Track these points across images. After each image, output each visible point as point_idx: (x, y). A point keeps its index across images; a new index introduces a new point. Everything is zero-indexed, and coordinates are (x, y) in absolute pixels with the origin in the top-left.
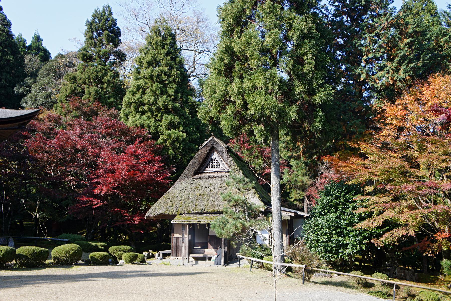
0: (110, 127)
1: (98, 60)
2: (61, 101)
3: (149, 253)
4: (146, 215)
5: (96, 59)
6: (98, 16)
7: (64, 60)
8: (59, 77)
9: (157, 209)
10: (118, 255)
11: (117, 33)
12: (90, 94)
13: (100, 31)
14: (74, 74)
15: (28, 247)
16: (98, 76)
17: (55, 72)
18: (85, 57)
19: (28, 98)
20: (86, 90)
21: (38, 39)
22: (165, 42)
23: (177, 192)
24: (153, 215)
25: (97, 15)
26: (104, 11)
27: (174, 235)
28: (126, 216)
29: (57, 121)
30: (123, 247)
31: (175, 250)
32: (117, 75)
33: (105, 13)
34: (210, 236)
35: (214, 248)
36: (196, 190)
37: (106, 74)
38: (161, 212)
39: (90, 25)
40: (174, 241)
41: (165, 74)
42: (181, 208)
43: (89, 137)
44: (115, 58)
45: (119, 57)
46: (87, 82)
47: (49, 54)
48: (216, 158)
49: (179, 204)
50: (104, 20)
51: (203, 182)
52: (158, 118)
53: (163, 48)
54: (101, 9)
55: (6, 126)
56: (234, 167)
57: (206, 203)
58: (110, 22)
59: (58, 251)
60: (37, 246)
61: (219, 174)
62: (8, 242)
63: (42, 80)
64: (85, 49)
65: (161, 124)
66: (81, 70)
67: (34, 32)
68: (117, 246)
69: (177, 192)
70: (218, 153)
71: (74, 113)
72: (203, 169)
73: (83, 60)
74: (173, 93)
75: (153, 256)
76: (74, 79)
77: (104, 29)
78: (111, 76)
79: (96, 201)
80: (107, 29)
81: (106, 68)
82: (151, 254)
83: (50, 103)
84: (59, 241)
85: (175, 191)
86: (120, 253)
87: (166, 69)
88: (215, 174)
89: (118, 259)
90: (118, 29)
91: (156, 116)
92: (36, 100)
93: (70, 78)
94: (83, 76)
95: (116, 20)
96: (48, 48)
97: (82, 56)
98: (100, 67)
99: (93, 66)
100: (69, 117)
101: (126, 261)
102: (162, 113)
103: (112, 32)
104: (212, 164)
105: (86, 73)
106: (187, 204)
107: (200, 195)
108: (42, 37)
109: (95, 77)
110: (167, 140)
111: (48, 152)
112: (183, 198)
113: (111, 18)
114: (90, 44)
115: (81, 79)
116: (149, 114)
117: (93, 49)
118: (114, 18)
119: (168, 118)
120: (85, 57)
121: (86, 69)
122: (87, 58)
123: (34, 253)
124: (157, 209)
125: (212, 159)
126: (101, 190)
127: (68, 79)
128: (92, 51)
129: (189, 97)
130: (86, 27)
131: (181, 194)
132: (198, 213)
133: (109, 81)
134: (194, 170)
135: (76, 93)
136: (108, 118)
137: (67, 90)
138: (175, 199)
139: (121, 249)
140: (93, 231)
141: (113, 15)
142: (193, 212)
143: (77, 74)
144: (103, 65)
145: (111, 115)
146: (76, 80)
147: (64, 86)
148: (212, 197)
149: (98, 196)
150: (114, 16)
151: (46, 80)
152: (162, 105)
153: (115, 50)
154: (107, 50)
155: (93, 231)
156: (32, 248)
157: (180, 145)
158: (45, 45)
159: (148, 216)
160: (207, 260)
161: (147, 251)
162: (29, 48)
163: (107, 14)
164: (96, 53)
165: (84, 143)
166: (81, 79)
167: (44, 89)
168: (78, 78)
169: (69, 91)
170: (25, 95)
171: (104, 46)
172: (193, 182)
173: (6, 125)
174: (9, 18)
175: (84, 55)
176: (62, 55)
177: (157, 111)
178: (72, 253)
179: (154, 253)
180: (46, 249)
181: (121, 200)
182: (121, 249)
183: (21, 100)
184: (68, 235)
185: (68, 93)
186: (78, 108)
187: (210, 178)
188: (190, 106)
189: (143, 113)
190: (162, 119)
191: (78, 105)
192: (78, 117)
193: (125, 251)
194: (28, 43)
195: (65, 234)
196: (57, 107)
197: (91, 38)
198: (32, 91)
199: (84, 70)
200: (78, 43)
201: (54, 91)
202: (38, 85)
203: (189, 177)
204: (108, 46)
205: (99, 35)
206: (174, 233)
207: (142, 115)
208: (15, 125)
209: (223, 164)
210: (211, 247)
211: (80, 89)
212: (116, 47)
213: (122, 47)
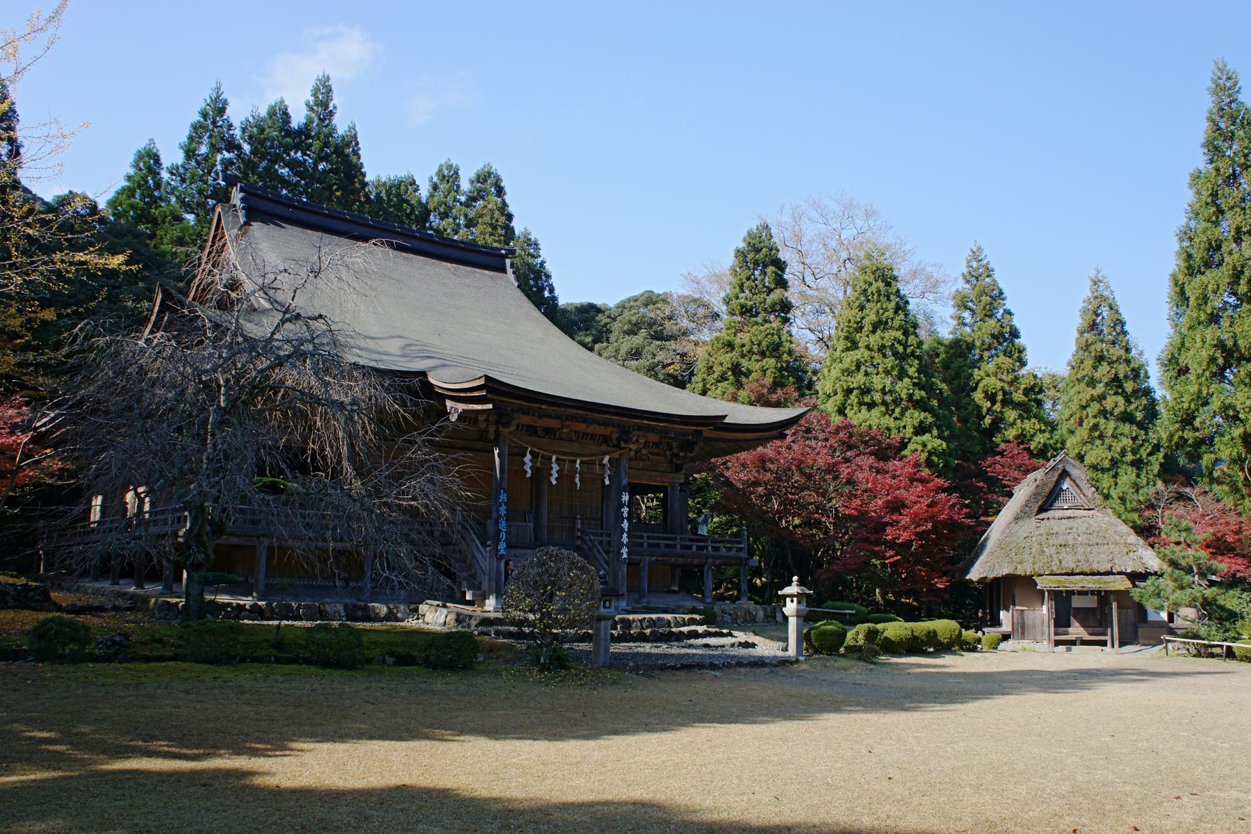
22: (1103, 330)
41: (899, 342)
53: (889, 300)
55: (595, 415)
77: (762, 261)
87: (899, 334)
91: (893, 411)
112: (1034, 550)
134: (1037, 506)
148: (1080, 550)
177: (892, 405)
189: (871, 406)
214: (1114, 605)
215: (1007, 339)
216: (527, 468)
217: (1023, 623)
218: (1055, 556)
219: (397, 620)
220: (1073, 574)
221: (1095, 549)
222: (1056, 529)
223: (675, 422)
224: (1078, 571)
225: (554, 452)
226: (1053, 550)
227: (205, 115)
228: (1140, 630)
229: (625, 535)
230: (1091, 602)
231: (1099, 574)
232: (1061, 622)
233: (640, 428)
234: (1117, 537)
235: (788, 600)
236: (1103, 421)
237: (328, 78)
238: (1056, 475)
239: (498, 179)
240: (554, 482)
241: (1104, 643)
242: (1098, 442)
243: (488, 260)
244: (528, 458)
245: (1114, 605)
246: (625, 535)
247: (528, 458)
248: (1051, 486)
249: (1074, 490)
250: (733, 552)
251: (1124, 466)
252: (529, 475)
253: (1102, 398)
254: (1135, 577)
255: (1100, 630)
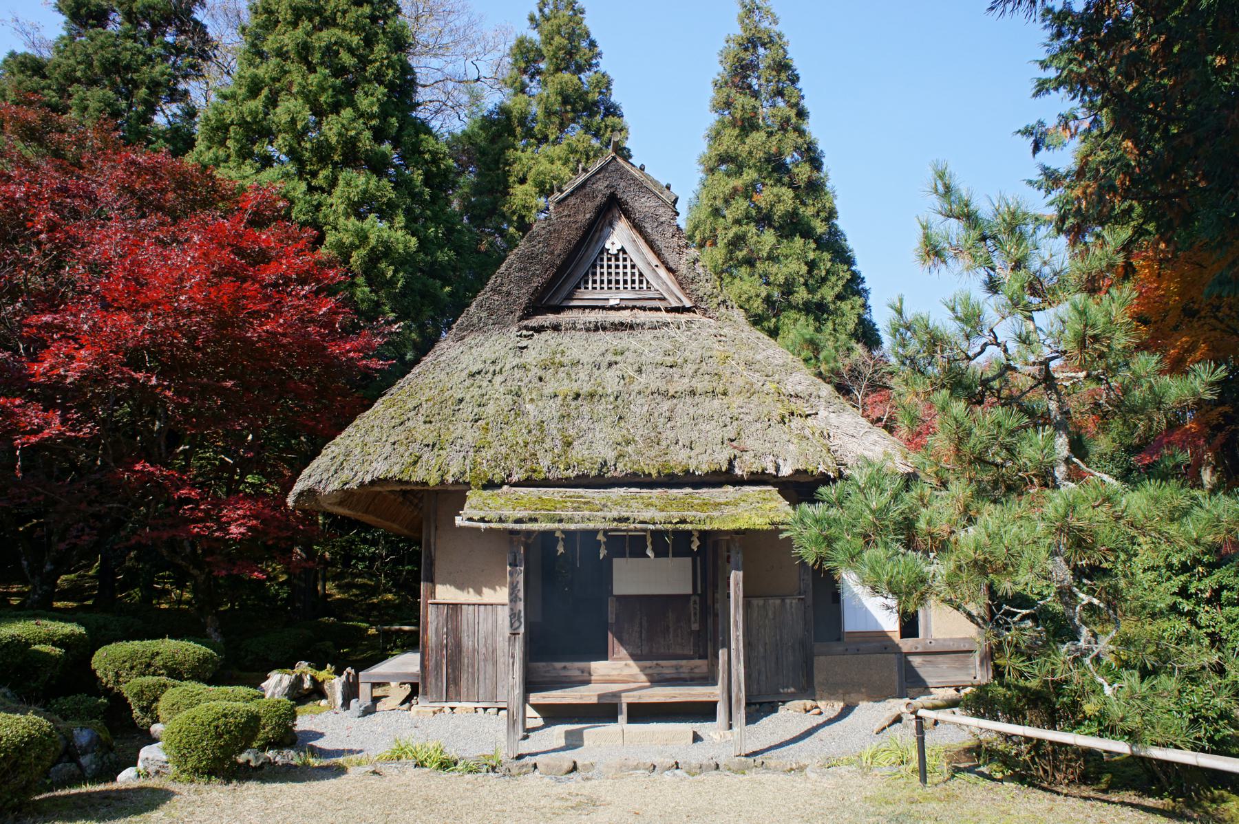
3: (299, 679)
4: (298, 487)
9: (358, 456)
10: (139, 695)
23: (455, 379)
24: (335, 485)
27: (433, 594)
28: (188, 500)
30: (169, 647)
31: (438, 666)
34: (623, 599)
35: (635, 657)
36: (548, 375)
38: (380, 469)
40: (433, 621)
42: (488, 453)
48: (623, 250)
49: (472, 436)
51: (573, 345)
52: (320, 181)
56: (709, 286)
57: (617, 435)
61: (642, 316)
65: (330, 201)
68: (136, 645)
69: (455, 379)
70: (638, 227)
72: (564, 293)
74: (375, 109)
75: (318, 692)
79: (34, 415)
82: (307, 684)
85: (443, 376)
86: (149, 680)
88: (625, 316)
89: (136, 713)
91: (314, 174)
101: (181, 759)
102: (335, 164)
104: (601, 273)
106: (516, 433)
107: (577, 396)
109: (108, 60)
110: (354, 247)
112: (491, 409)
116: (291, 168)
119: (359, 181)
120: (83, 11)
124: (358, 456)
125: (604, 250)
126: (71, 364)
129: (423, 136)
131: (475, 392)
132: (582, 482)
138: (448, 411)
139: (158, 661)
140: (48, 567)
142: (553, 475)
148: (639, 408)
149: (51, 395)
152: (340, 134)
155: (48, 567)
157: (396, 272)
159: (310, 493)
160: (623, 718)
161: (286, 664)
172: (524, 343)
179: (321, 675)
182: (158, 661)
187: (604, 329)
188: (426, 162)
189: (267, 161)
190: (333, 183)
193: (175, 673)
203: (501, 324)
206: (431, 580)
207: (263, 167)
209: (658, 276)
210: (623, 652)
214: (736, 578)
215: (591, 109)
217: (458, 645)
218: (553, 427)
220: (601, 481)
221: (685, 408)
222: (575, 353)
224: (622, 469)
226: (552, 409)
228: (820, 662)
230: (665, 577)
231: (690, 480)
232: (554, 643)
234: (756, 378)
236: (752, 229)
238: (591, 206)
241: (705, 712)
242: (744, 270)
245: (736, 578)
248: (571, 235)
249: (641, 255)
251: (793, 314)
253: (749, 192)
254: (801, 488)
255: (701, 665)
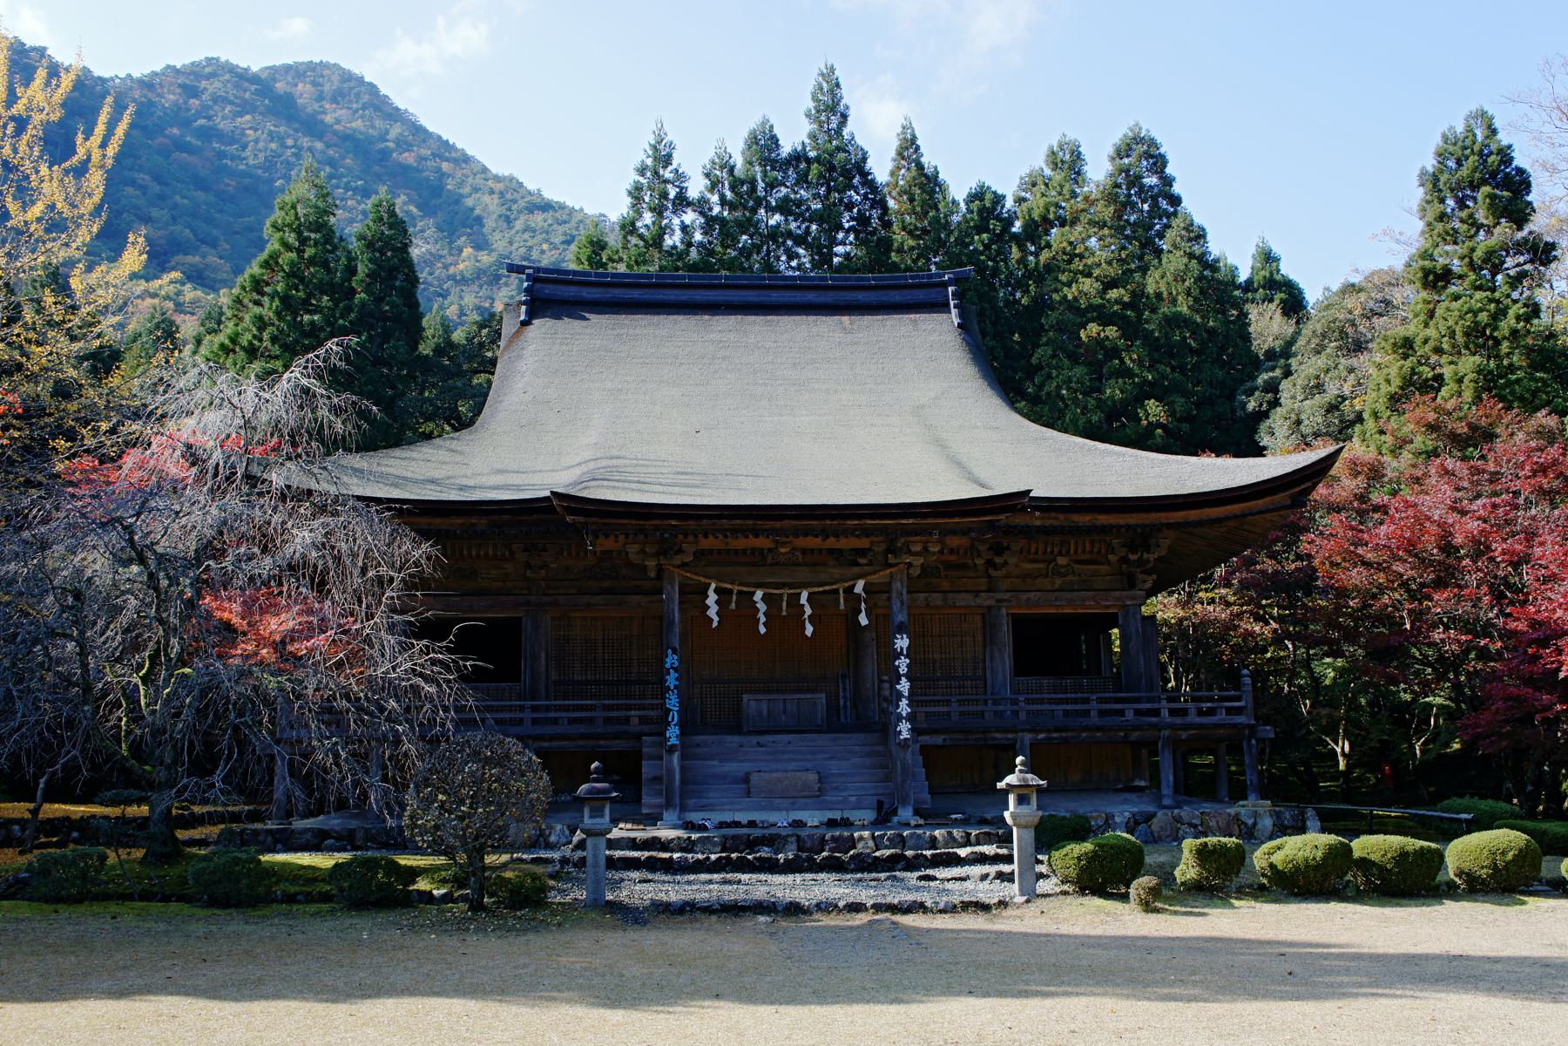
0: (1542, 470)
1: (1472, 276)
2: (1375, 415)
5: (1461, 277)
6: (1455, 150)
7: (1363, 297)
8: (1359, 347)
11: (1519, 183)
12: (1460, 381)
13: (1463, 192)
14: (1401, 331)
15: (1381, 837)
16: (1476, 323)
17: (1343, 334)
18: (1431, 277)
19: (1278, 421)
20: (1447, 372)
21: (1268, 258)
25: (1451, 148)
26: (1469, 130)
29: (1375, 473)
32: (1534, 310)
33: (1474, 135)
37: (1502, 313)
39: (1433, 183)
43: (1484, 506)
44: (1521, 259)
45: (1535, 254)
46: (1445, 346)
47: (1300, 292)
50: (1472, 158)
54: (1460, 128)
58: (1493, 158)
59: (1465, 852)
60: (1405, 835)
62: (1304, 821)
63: (1306, 366)
64: (1426, 255)
66: (1422, 317)
67: (1256, 240)
71: (1421, 441)
73: (1425, 285)
76: (1406, 346)
78: (1518, 318)
80: (1484, 182)
81: (1497, 295)
83: (1343, 425)
84: (1442, 818)
90: (1520, 171)
92: (1298, 422)
93: (1394, 344)
94: (1431, 332)
95: (1510, 147)
96: (1293, 276)
97: (1420, 275)
98: (1479, 295)
99: (1456, 298)
100: (1406, 456)
103: (1507, 183)
105: (1441, 322)
108: (1277, 250)
111: (1367, 564)
113: (1494, 147)
114: (1439, 235)
115: (1426, 341)
117: (1448, 248)
118: (1505, 143)
120: (1431, 277)
121: (1439, 312)
122: (1436, 279)
123: (1403, 855)
127: (1388, 347)
128: (1450, 257)
130: (1421, 190)
133: (1514, 333)
135: (1420, 385)
136: (1533, 444)
137: (1388, 381)
141: (1499, 136)
143: (1413, 329)
144: (1489, 289)
145: (1539, 433)
146: (1412, 347)
147: (1379, 370)
150: (1504, 138)
151: (1321, 362)
153: (1520, 235)
154: (1493, 241)
155: (1530, 788)
156: (1396, 841)
158: (1287, 269)
162: (1248, 286)
163: (1480, 138)
164: (1462, 258)
165: (1474, 526)
166: (1426, 341)
167: (1319, 388)
168: (1418, 341)
169: (1396, 382)
170: (1266, 415)
171: (1482, 232)
173: (1260, 502)
174: (1198, 220)
175: (1426, 273)
176: (1353, 285)
178: (1510, 856)
180: (1433, 845)
181: (1353, 660)
183: (1255, 431)
184: (1466, 801)
185: (1393, 389)
186: (1433, 428)
191: (1431, 417)
192: (1434, 453)
194: (1243, 277)
195: (1459, 801)
196: (1364, 433)
197: (1442, 217)
198: (1282, 400)
199: (1431, 314)
200: (1398, 242)
201: (1347, 390)
202: (1299, 382)
204: (1497, 230)
205: (1461, 204)
208: (1282, 498)
211: (1427, 373)
212: (1520, 228)
213: (1538, 224)
216: (713, 612)
219: (550, 846)
223: (926, 516)
225: (759, 586)
227: (642, 171)
229: (904, 703)
233: (915, 532)
235: (1012, 798)
237: (832, 70)
239: (1153, 143)
240: (763, 630)
243: (920, 295)
244: (712, 598)
246: (904, 703)
247: (712, 598)
250: (1221, 717)
252: (715, 624)
